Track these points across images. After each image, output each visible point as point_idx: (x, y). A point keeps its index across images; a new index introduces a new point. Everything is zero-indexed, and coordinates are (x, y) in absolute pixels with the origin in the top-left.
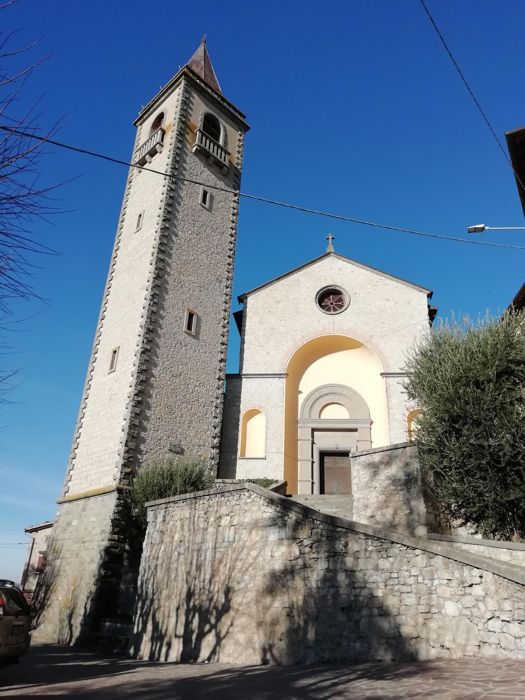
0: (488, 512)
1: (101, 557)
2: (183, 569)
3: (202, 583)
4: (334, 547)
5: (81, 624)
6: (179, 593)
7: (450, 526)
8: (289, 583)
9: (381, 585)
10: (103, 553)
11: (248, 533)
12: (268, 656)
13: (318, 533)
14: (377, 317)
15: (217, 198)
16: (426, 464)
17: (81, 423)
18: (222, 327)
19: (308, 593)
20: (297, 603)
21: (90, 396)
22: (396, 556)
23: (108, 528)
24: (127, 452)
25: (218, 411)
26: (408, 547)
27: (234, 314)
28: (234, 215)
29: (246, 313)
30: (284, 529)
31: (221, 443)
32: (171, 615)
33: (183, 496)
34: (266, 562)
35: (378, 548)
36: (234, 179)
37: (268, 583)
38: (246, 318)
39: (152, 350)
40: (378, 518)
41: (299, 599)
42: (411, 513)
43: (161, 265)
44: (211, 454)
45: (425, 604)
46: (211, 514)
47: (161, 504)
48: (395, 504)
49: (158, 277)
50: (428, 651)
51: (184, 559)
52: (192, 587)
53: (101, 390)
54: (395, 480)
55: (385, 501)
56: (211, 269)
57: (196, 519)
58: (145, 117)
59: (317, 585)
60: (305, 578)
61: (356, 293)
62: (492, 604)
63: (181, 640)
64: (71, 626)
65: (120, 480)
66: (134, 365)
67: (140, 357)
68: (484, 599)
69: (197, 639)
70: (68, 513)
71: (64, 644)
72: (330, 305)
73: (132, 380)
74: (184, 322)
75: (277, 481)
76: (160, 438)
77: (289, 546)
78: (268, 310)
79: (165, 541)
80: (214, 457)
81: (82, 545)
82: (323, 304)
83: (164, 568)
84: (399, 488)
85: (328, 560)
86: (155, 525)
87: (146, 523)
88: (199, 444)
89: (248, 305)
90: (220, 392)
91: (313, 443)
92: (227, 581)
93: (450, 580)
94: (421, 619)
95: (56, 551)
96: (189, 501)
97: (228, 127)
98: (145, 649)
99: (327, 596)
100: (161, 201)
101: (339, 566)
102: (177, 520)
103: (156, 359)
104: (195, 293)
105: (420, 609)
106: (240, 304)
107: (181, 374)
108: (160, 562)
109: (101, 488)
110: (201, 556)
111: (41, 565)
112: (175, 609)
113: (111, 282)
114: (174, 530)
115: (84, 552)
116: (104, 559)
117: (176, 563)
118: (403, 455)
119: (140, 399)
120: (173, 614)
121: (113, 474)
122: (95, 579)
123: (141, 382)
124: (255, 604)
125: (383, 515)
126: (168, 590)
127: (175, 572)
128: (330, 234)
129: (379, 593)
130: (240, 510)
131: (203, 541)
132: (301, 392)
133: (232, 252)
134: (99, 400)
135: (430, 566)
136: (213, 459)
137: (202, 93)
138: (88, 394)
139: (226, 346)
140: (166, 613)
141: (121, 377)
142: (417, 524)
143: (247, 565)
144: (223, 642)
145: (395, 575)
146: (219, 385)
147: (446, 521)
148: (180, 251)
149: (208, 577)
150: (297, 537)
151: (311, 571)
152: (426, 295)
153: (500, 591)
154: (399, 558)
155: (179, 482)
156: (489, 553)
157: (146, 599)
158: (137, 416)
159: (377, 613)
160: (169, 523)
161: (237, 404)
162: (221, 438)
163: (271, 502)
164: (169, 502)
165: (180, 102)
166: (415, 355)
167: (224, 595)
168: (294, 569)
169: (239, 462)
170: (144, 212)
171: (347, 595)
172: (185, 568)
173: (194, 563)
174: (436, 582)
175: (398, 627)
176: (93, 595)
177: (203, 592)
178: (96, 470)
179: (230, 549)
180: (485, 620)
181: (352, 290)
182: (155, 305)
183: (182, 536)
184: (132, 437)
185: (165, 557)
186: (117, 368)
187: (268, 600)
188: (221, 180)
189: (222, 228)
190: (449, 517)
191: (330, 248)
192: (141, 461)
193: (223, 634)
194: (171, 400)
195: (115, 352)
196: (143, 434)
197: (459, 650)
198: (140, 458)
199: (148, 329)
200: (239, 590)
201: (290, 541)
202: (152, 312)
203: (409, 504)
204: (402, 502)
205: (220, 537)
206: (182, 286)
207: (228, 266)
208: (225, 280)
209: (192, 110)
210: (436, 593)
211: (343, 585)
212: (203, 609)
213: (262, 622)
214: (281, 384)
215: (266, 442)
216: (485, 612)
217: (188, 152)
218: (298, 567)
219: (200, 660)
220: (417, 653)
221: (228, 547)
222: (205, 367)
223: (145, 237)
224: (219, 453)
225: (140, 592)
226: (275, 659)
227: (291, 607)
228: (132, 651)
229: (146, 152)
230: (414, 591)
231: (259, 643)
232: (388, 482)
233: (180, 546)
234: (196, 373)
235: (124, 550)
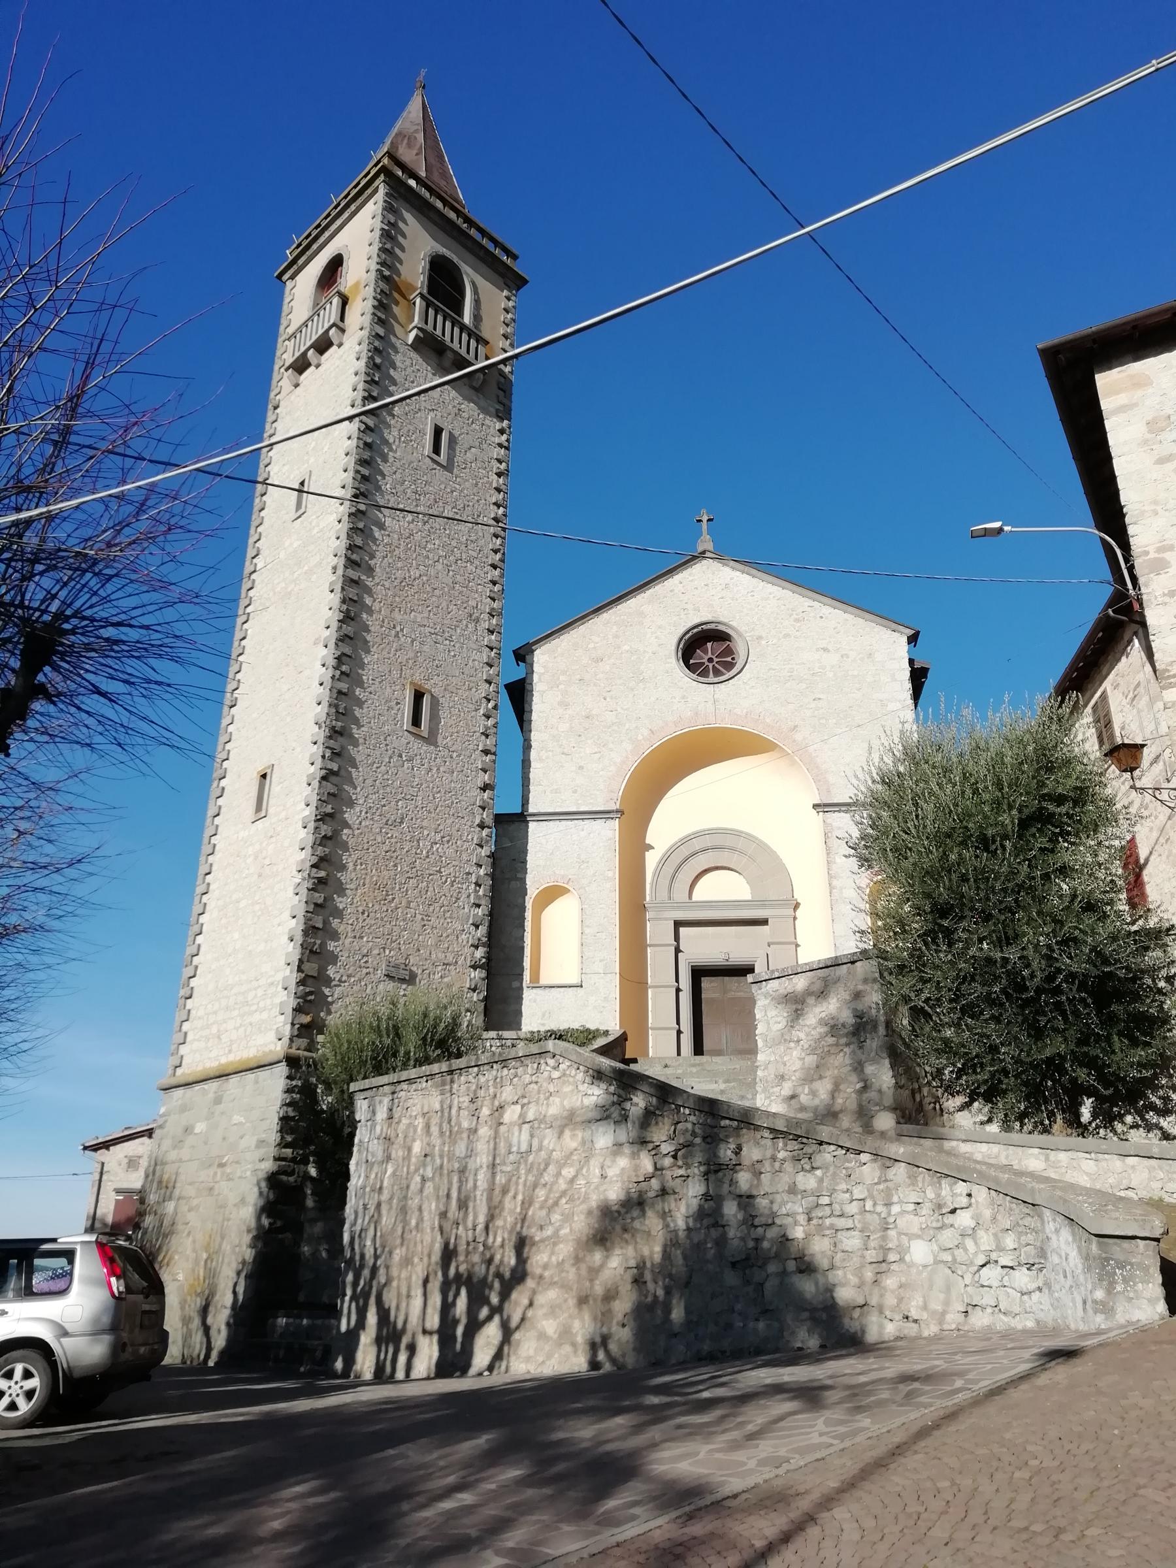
0: (1006, 1081)
1: (261, 1193)
2: (432, 1208)
3: (470, 1233)
4: (715, 1155)
5: (228, 1324)
6: (426, 1252)
7: (941, 1110)
8: (637, 1224)
9: (802, 1219)
10: (263, 1184)
11: (556, 1135)
12: (601, 1356)
13: (687, 1130)
14: (804, 686)
15: (463, 441)
16: (892, 994)
17: (199, 925)
18: (483, 718)
19: (671, 1240)
20: (651, 1258)
21: (214, 868)
22: (824, 1167)
23: (273, 1137)
24: (301, 983)
25: (481, 893)
27: (506, 686)
28: (499, 475)
29: (531, 684)
30: (623, 1126)
31: (489, 957)
32: (413, 1293)
33: (426, 1069)
34: (592, 1187)
35: (795, 1153)
36: (498, 396)
37: (596, 1226)
38: (533, 695)
39: (343, 773)
40: (804, 1099)
41: (654, 1250)
42: (865, 1088)
43: (352, 593)
44: (471, 980)
45: (877, 1247)
46: (482, 1101)
47: (382, 1086)
52: (452, 1241)
54: (835, 1025)
55: (817, 1067)
56: (457, 594)
57: (454, 1111)
58: (300, 262)
59: (687, 1223)
60: (664, 1212)
61: (760, 638)
62: (986, 1240)
63: (435, 1338)
64: (207, 1329)
65: (291, 1040)
66: (308, 805)
67: (319, 788)
69: (465, 1334)
70: (184, 1109)
71: (195, 1363)
72: (707, 663)
73: (305, 836)
74: (404, 709)
75: (607, 1031)
76: (366, 951)
77: (634, 1155)
79: (393, 1156)
80: (476, 986)
81: (219, 1171)
82: (692, 661)
83: (394, 1206)
84: (843, 1041)
85: (707, 1180)
86: (373, 1127)
87: (354, 1124)
88: (446, 962)
89: (536, 667)
90: (485, 852)
91: (678, 950)
92: (519, 1226)
93: (918, 1204)
95: (164, 1184)
96: (438, 1079)
97: (482, 283)
99: (706, 1243)
100: (347, 455)
101: (726, 1188)
102: (416, 1116)
104: (426, 648)
105: (868, 1257)
106: (518, 665)
108: (385, 1197)
109: (251, 1055)
110: (467, 1181)
111: (134, 1212)
112: (420, 1282)
113: (245, 626)
114: (411, 1134)
115: (224, 1184)
118: (851, 976)
119: (322, 874)
120: (418, 1293)
121: (275, 1027)
122: (251, 1236)
123: (324, 840)
124: (573, 1265)
125: (814, 1093)
126: (404, 1249)
127: (417, 1213)
128: (704, 511)
129: (798, 1233)
130: (539, 1092)
131: (469, 1153)
132: (650, 847)
133: (499, 556)
135: (886, 1181)
136: (474, 990)
137: (423, 209)
138: (211, 865)
139: (494, 757)
140: (404, 1291)
141: (279, 828)
142: (878, 1108)
143: (557, 1195)
144: (517, 1336)
145: (825, 1200)
147: (933, 1100)
148: (391, 561)
149: (481, 1219)
150: (648, 1139)
151: (676, 1200)
152: (905, 639)
153: (999, 1217)
154: (832, 1169)
155: (411, 1041)
156: (1007, 1157)
157: (362, 1266)
158: (319, 909)
161: (519, 875)
162: (489, 946)
163: (598, 1075)
164: (399, 1082)
165: (378, 233)
166: (870, 782)
167: (514, 1251)
168: (645, 1196)
169: (528, 995)
170: (310, 476)
171: (743, 1239)
172: (437, 1206)
173: (454, 1194)
174: (895, 1209)
175: (830, 1289)
176: (250, 1267)
177: (474, 1248)
179: (522, 1166)
180: (976, 1268)
181: (753, 629)
182: (344, 677)
183: (428, 1144)
184: (311, 951)
185: (396, 1187)
186: (271, 811)
187: (597, 1256)
188: (471, 400)
189: (476, 506)
190: (939, 1094)
192: (330, 999)
193: (514, 1322)
194: (386, 873)
195: (264, 776)
196: (331, 946)
197: (934, 1322)
198: (328, 994)
199: (333, 729)
200: (542, 1241)
201: (636, 1148)
202: (340, 692)
203: (862, 1071)
205: (502, 1144)
206: (397, 635)
208: (486, 616)
209: (403, 249)
210: (896, 1227)
211: (733, 1222)
212: (475, 1280)
213: (587, 1297)
214: (610, 830)
215: (582, 952)
217: (398, 343)
218: (651, 1194)
219: (473, 1371)
220: (863, 1332)
221: (519, 1163)
222: (452, 803)
223: (315, 531)
224: (487, 978)
225: (349, 1256)
226: (613, 1361)
227: (641, 1267)
228: (339, 1365)
229: (308, 344)
230: (859, 1226)
233: (424, 1165)
234: (433, 815)
235: (307, 1177)
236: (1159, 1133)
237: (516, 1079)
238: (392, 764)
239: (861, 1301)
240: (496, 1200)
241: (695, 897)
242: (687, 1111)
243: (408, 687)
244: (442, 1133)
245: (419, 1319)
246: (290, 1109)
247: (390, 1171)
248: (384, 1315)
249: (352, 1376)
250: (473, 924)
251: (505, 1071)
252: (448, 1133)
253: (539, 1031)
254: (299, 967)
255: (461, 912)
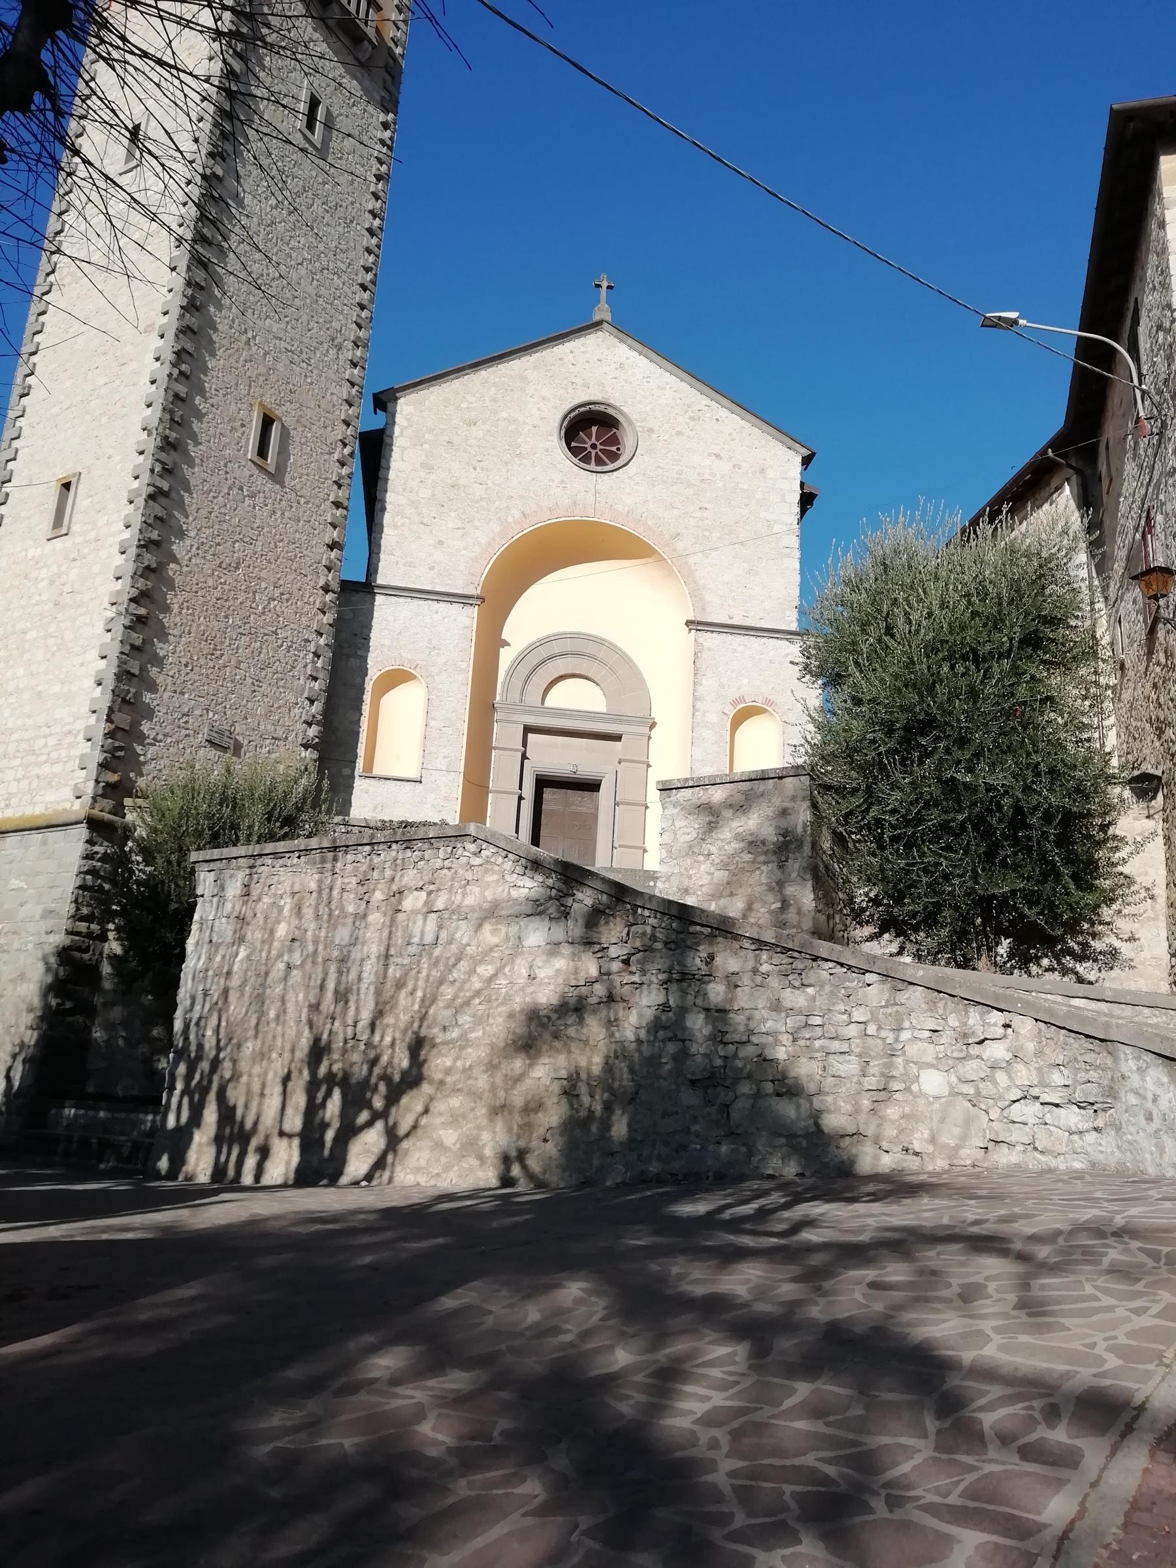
1: (48, 969)
2: (298, 1000)
6: (288, 1047)
9: (786, 1039)
10: (52, 960)
11: (472, 929)
12: (516, 1171)
14: (692, 492)
19: (615, 1052)
24: (110, 735)
25: (319, 664)
26: (850, 967)
30: (562, 923)
31: (322, 736)
32: (267, 1092)
34: (515, 988)
39: (173, 495)
41: (594, 1062)
47: (235, 858)
48: (749, 890)
49: (191, 307)
50: (877, 1158)
51: (303, 978)
52: (325, 1036)
53: (26, 578)
55: (728, 883)
57: (335, 893)
60: (610, 1021)
61: (651, 430)
62: (1024, 1075)
63: (296, 1142)
65: (94, 799)
66: (127, 527)
67: (145, 507)
68: (1007, 1067)
69: (336, 1139)
72: (589, 449)
73: (124, 563)
74: (249, 435)
77: (574, 957)
78: (446, 438)
79: (249, 936)
83: (247, 995)
84: (762, 858)
89: (399, 419)
90: (328, 618)
91: (524, 757)
92: (416, 1025)
94: (865, 1102)
96: (316, 856)
98: (198, 1160)
103: (183, 520)
104: (280, 366)
106: (375, 413)
107: (238, 563)
108: (235, 981)
109: (37, 813)
110: (348, 971)
112: (279, 1080)
116: (57, 974)
117: (281, 986)
119: (142, 611)
121: (72, 783)
122: (32, 1016)
123: (147, 572)
128: (604, 276)
129: (781, 1054)
132: (505, 644)
133: (369, 276)
134: (23, 602)
139: (345, 512)
140: (256, 1087)
141: (86, 551)
143: (468, 994)
144: (405, 1144)
146: (325, 603)
149: (366, 1015)
151: (624, 1008)
153: (1048, 1051)
154: (828, 988)
157: (199, 1057)
159: (771, 1091)
160: (260, 899)
161: (360, 653)
164: (261, 855)
167: (407, 1053)
169: (359, 785)
171: (707, 1056)
172: (306, 997)
173: (331, 986)
174: (906, 1035)
178: (21, 773)
180: (1007, 1103)
181: (645, 420)
182: (183, 379)
184: (124, 701)
186: (75, 528)
187: (518, 1064)
188: (354, 77)
190: (848, 923)
191: (603, 311)
192: (142, 758)
194: (215, 623)
195: (67, 486)
196: (147, 697)
199: (165, 438)
200: (445, 1043)
202: (177, 396)
203: (780, 891)
204: (765, 888)
205: (399, 934)
206: (248, 342)
207: (358, 309)
210: (904, 1054)
211: (699, 1037)
212: (353, 1081)
214: (467, 618)
215: (425, 745)
216: (1008, 1089)
218: (594, 1000)
219: (344, 1180)
221: (421, 956)
222: (296, 556)
225: (180, 1045)
226: (531, 1176)
228: (164, 1164)
230: (857, 1050)
231: (494, 1147)
232: (737, 846)
233: (291, 951)
234: (273, 566)
236: (1074, 977)
237: (422, 863)
238: (231, 497)
239: (851, 1129)
240: (387, 994)
241: (547, 704)
242: (647, 913)
243: (256, 408)
244: (318, 917)
245: (275, 1119)
246: (89, 877)
247: (242, 954)
248: (227, 1114)
249: (181, 1178)
250: (307, 698)
251: (409, 853)
252: (326, 917)
253: (391, 821)
254: (108, 715)
255: (296, 683)
